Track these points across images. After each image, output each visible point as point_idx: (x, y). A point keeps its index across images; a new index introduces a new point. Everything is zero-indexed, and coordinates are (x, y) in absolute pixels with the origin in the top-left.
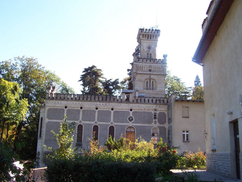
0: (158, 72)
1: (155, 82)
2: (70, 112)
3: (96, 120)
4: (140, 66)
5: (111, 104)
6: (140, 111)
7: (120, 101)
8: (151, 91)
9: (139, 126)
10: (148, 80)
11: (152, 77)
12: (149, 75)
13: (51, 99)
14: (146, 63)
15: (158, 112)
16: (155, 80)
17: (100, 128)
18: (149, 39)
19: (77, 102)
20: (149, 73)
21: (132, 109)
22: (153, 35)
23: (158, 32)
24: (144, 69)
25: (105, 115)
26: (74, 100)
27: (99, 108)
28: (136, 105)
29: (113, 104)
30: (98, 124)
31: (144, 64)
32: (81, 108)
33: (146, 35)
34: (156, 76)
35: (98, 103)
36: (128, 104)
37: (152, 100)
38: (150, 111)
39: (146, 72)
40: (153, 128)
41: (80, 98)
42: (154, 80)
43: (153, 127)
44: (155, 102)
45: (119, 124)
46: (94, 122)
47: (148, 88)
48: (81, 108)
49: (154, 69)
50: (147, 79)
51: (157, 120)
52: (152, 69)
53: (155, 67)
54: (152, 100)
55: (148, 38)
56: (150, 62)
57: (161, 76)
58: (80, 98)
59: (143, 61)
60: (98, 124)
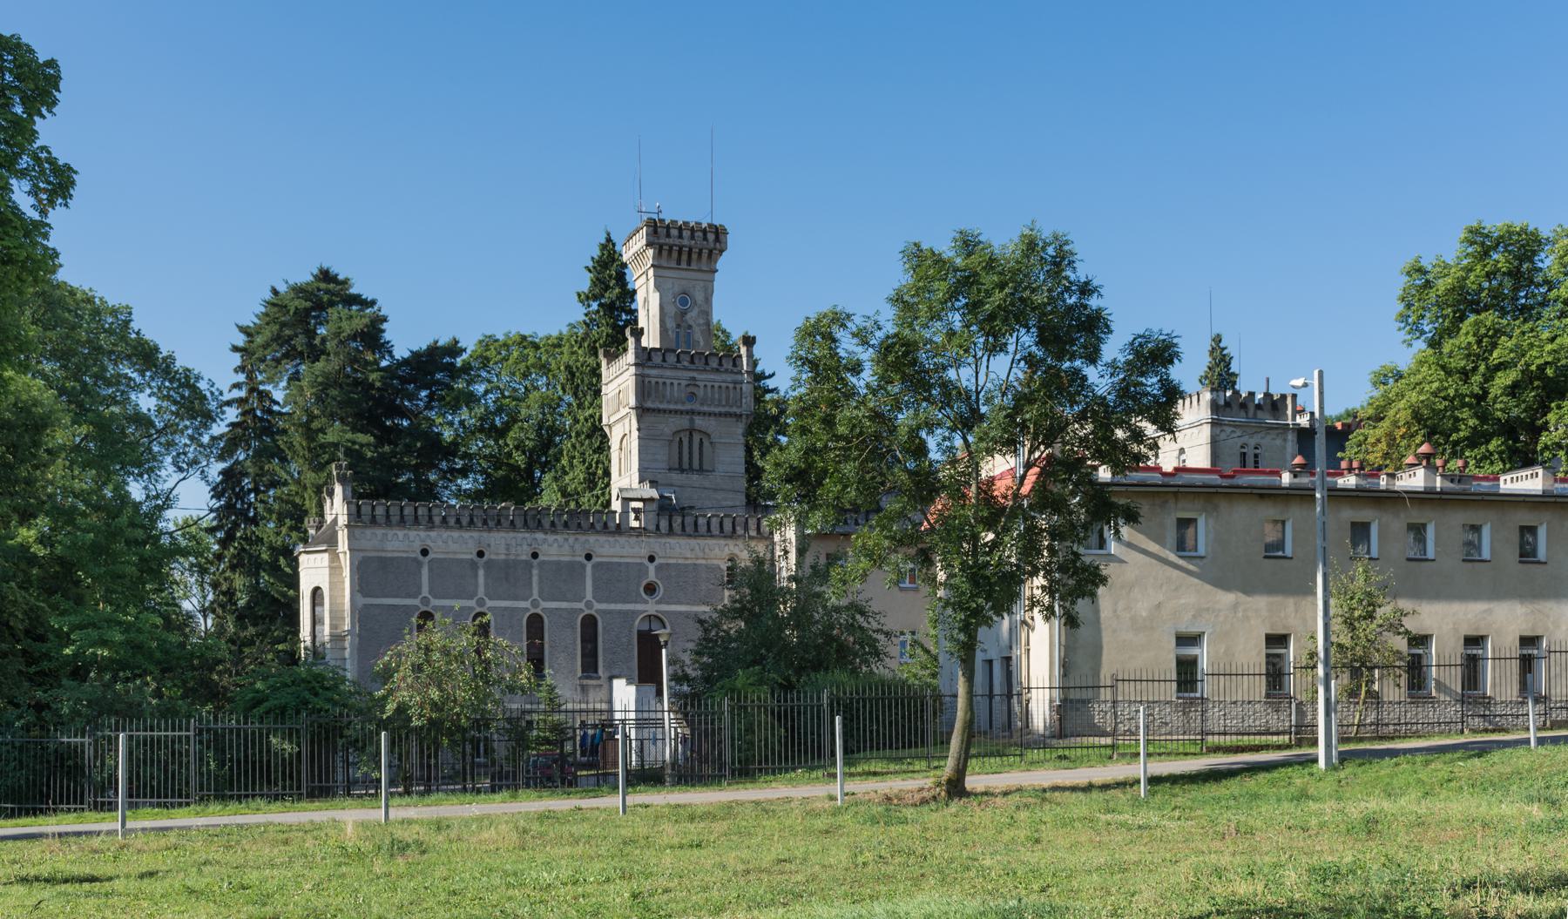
1: (711, 443)
2: (440, 569)
3: (589, 596)
4: (653, 381)
5: (582, 538)
6: (680, 561)
8: (695, 477)
9: (680, 613)
10: (682, 435)
11: (699, 422)
12: (688, 417)
14: (676, 368)
16: (709, 435)
17: (550, 622)
18: (684, 265)
19: (466, 535)
20: (688, 407)
22: (701, 250)
23: (722, 237)
24: (668, 393)
25: (565, 577)
26: (452, 527)
28: (668, 540)
29: (592, 538)
31: (668, 373)
32: (535, 555)
33: (671, 247)
34: (712, 418)
35: (540, 536)
37: (721, 524)
38: (715, 562)
39: (676, 403)
42: (705, 433)
44: (731, 529)
45: (612, 607)
46: (427, 595)
47: (686, 466)
48: (535, 555)
49: (705, 393)
50: (679, 431)
52: (700, 393)
53: (709, 384)
54: (721, 524)
55: (679, 262)
56: (693, 367)
57: (729, 419)
58: (475, 520)
59: (664, 360)
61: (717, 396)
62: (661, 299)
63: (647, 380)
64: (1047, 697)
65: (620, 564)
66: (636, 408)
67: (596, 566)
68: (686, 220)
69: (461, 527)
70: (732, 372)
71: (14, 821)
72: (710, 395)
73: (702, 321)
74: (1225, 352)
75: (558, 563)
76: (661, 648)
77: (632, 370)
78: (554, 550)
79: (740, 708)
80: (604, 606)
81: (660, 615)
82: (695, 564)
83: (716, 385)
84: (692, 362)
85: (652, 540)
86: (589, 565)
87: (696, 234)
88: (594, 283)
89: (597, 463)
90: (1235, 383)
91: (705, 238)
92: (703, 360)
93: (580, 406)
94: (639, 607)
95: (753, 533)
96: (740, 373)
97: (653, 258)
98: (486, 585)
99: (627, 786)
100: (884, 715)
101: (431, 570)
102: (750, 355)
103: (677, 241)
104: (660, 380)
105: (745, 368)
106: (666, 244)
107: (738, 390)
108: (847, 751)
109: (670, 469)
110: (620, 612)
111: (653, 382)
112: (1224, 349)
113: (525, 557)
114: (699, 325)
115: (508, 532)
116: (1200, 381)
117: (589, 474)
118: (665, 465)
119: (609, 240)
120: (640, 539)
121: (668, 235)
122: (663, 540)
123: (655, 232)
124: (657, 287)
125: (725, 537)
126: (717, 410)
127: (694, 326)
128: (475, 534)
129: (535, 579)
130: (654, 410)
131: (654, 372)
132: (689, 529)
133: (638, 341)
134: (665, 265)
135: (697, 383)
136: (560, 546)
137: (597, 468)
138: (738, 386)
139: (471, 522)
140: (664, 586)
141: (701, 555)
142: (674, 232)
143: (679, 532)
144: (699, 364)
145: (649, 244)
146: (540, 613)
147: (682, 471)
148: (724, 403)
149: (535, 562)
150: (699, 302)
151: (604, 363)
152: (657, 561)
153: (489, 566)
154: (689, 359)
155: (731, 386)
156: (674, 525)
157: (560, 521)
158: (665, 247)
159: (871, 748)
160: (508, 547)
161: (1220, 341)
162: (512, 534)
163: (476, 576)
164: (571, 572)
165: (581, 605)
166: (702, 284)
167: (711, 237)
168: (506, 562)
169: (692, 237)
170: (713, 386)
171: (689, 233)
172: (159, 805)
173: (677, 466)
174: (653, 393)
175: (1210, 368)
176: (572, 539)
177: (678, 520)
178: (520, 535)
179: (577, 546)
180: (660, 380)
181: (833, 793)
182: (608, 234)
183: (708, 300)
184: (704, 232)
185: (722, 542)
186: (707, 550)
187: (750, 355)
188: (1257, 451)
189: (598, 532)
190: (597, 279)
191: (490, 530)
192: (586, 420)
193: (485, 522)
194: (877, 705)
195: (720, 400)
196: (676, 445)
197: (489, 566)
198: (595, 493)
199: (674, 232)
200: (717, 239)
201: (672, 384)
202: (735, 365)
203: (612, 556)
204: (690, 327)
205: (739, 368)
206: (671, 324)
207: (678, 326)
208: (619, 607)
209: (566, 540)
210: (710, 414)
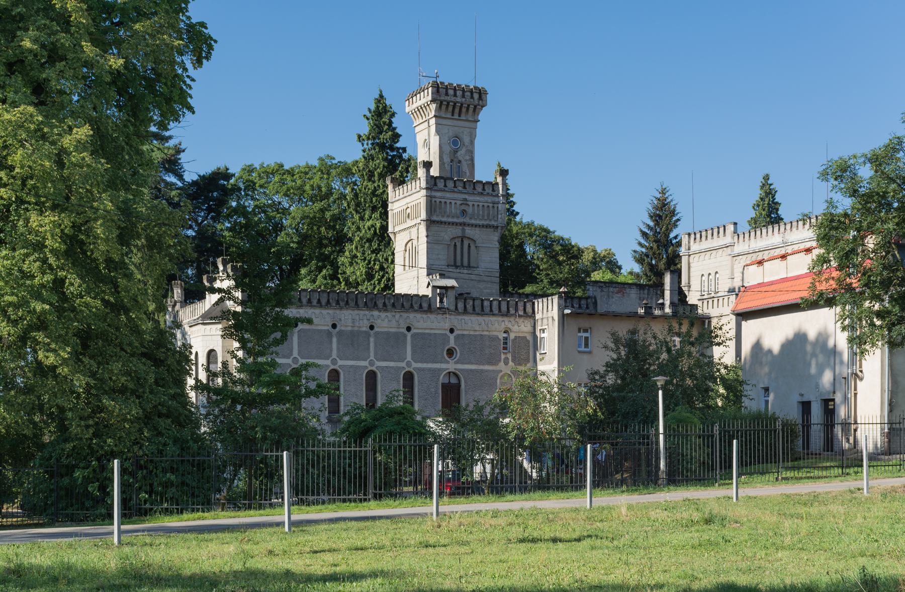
0: (483, 219)
3: (409, 358)
4: (438, 200)
5: (405, 315)
6: (472, 333)
7: (426, 309)
9: (471, 370)
10: (456, 241)
11: (469, 232)
14: (454, 192)
15: (512, 336)
16: (474, 241)
17: (382, 376)
18: (456, 116)
19: (325, 312)
20: (461, 220)
22: (469, 106)
23: (483, 96)
26: (315, 306)
28: (464, 317)
29: (412, 315)
31: (448, 195)
32: (372, 327)
33: (448, 103)
35: (376, 313)
38: (495, 333)
39: (453, 217)
41: (328, 301)
43: (501, 371)
44: (506, 310)
45: (425, 365)
47: (459, 263)
48: (372, 327)
49: (473, 210)
50: (454, 238)
51: (509, 356)
52: (470, 210)
53: (476, 204)
55: (453, 115)
56: (465, 191)
59: (445, 186)
61: (481, 213)
62: (440, 141)
63: (434, 200)
64: (879, 430)
65: (430, 334)
66: (427, 220)
67: (414, 336)
68: (459, 83)
69: (321, 306)
70: (492, 195)
71: (262, 512)
72: (476, 212)
73: (468, 158)
74: (771, 187)
75: (388, 333)
76: (658, 389)
77: (424, 192)
78: (385, 323)
79: (725, 432)
80: (420, 365)
81: (457, 372)
83: (481, 204)
84: (464, 187)
85: (452, 317)
86: (409, 335)
87: (466, 94)
88: (372, 128)
89: (375, 260)
90: (777, 210)
91: (472, 97)
93: (362, 218)
94: (443, 366)
95: (521, 313)
96: (497, 196)
97: (436, 111)
98: (338, 349)
99: (594, 487)
100: (767, 440)
101: (299, 338)
102: (505, 184)
103: (453, 99)
104: (443, 201)
105: (501, 192)
106: (445, 101)
107: (496, 209)
108: (741, 464)
109: (448, 266)
110: (430, 369)
111: (438, 202)
112: (771, 185)
113: (365, 329)
114: (466, 160)
115: (354, 310)
116: (753, 207)
117: (368, 268)
118: (445, 263)
119: (381, 96)
120: (445, 316)
121: (447, 94)
122: (460, 317)
123: (438, 91)
124: (438, 132)
125: (502, 315)
126: (481, 223)
127: (463, 161)
128: (331, 312)
130: (438, 222)
131: (438, 194)
132: (478, 309)
133: (428, 171)
134: (444, 116)
135: (468, 203)
136: (389, 321)
137: (375, 264)
138: (496, 206)
139: (328, 302)
141: (486, 328)
142: (451, 92)
144: (469, 188)
145: (433, 101)
147: (457, 267)
148: (486, 218)
149: (372, 332)
150: (466, 144)
151: (390, 187)
152: (456, 332)
153: (340, 334)
155: (491, 205)
156: (468, 306)
159: (759, 463)
160: (353, 321)
161: (768, 179)
162: (356, 312)
163: (331, 342)
164: (398, 339)
165: (403, 364)
166: (468, 130)
167: (476, 96)
168: (352, 332)
169: (463, 96)
170: (478, 205)
171: (461, 92)
172: (344, 501)
174: (438, 211)
175: (762, 199)
176: (398, 315)
177: (470, 303)
178: (362, 312)
179: (401, 321)
180: (443, 201)
181: (730, 495)
182: (381, 92)
183: (472, 142)
184: (471, 92)
185: (500, 319)
186: (490, 325)
187: (505, 184)
189: (416, 311)
190: (375, 125)
191: (341, 308)
192: (369, 229)
193: (338, 303)
194: (758, 434)
195: (483, 216)
196: (452, 248)
198: (372, 282)
199: (451, 92)
200: (480, 98)
201: (450, 203)
202: (493, 190)
203: (425, 329)
204: (460, 162)
205: (496, 193)
206: (447, 160)
207: (452, 161)
208: (430, 366)
210: (476, 226)
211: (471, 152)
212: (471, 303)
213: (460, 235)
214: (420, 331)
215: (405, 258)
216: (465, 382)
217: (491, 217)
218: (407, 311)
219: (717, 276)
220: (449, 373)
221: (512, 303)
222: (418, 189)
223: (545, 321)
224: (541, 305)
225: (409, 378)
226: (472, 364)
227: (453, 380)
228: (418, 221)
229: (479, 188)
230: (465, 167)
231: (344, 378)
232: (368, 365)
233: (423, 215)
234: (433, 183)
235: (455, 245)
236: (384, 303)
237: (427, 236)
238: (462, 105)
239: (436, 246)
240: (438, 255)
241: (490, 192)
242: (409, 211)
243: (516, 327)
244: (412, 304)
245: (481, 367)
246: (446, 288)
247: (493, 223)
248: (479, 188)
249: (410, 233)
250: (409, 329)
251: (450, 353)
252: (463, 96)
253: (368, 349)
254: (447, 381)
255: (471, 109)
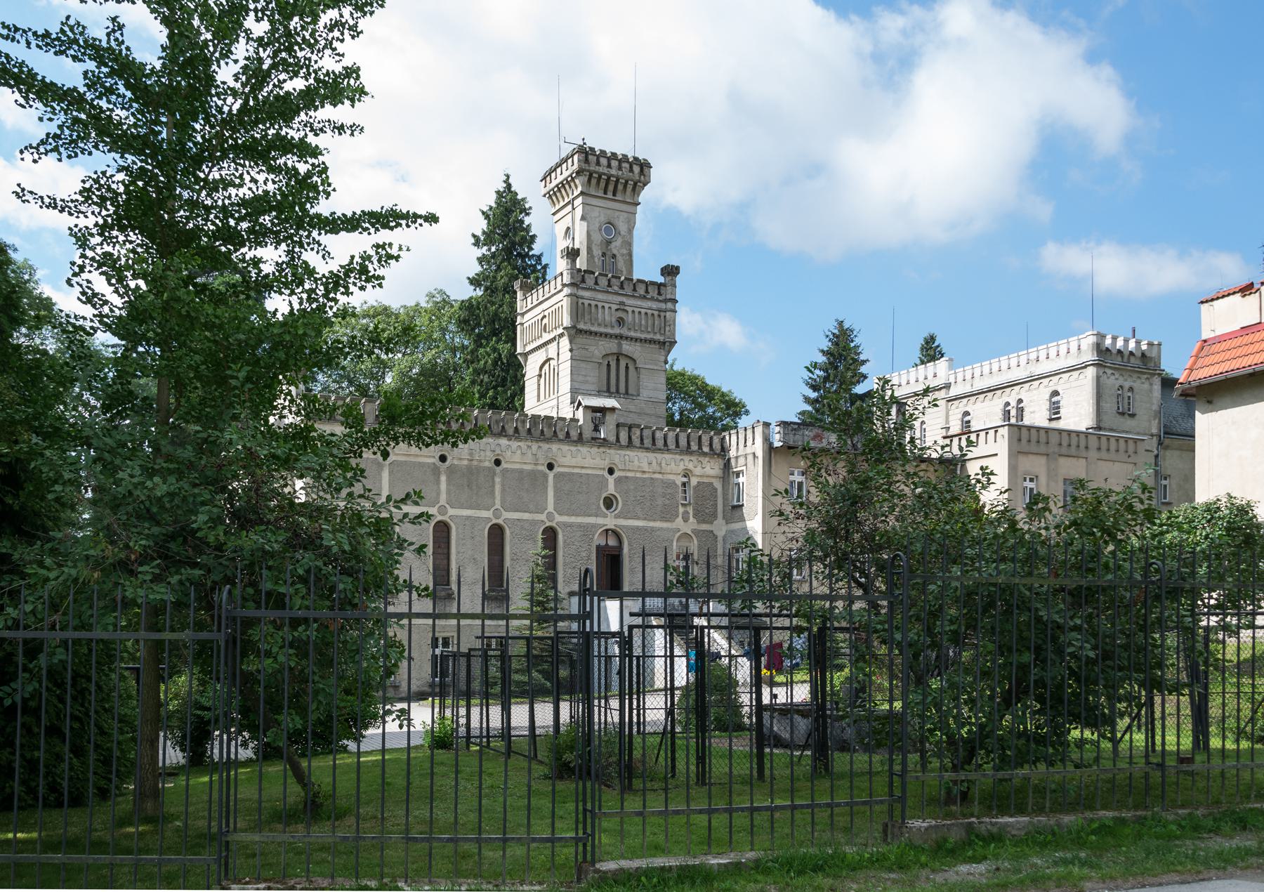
3: (550, 508)
4: (586, 302)
5: (545, 446)
6: (639, 475)
7: (575, 439)
9: (638, 528)
10: (610, 358)
11: (627, 347)
13: (575, 441)
15: (694, 481)
16: (634, 361)
18: (610, 195)
20: (617, 331)
21: (500, 458)
22: (627, 182)
23: (646, 170)
27: (559, 466)
28: (628, 453)
29: (555, 447)
30: (503, 518)
31: (600, 296)
32: (498, 463)
33: (600, 177)
36: (602, 449)
38: (671, 477)
40: (679, 534)
42: (631, 358)
44: (686, 444)
45: (573, 519)
47: (613, 389)
48: (498, 463)
50: (607, 355)
53: (637, 310)
55: (605, 193)
60: (503, 518)
61: (643, 322)
65: (581, 475)
70: (658, 300)
73: (625, 252)
75: (521, 471)
80: (565, 519)
82: (652, 479)
84: (622, 287)
85: (612, 451)
86: (551, 475)
92: (632, 287)
94: (600, 521)
95: (706, 449)
98: (448, 492)
101: (391, 473)
103: (606, 170)
106: (596, 172)
110: (580, 525)
114: (623, 255)
122: (622, 452)
126: (643, 336)
129: (498, 488)
130: (586, 332)
131: (586, 294)
132: (647, 442)
135: (626, 308)
136: (523, 454)
140: (623, 501)
143: (638, 445)
144: (628, 289)
146: (502, 523)
149: (498, 469)
150: (622, 233)
152: (617, 474)
153: (452, 471)
154: (619, 284)
156: (633, 437)
157: (523, 427)
158: (595, 175)
163: (438, 482)
165: (543, 517)
167: (636, 169)
168: (469, 468)
170: (640, 312)
171: (617, 163)
173: (605, 389)
176: (535, 446)
179: (540, 454)
180: (593, 303)
183: (630, 231)
186: (663, 465)
188: (967, 418)
196: (605, 368)
197: (452, 471)
201: (603, 307)
204: (614, 256)
206: (597, 252)
207: (604, 255)
208: (580, 520)
209: (529, 447)
210: (636, 340)
211: (628, 244)
212: (638, 433)
213: (615, 351)
214: (566, 470)
215: (539, 385)
216: (629, 544)
217: (656, 330)
218: (548, 440)
219: (924, 426)
220: (607, 531)
221: (694, 436)
222: (559, 287)
223: (741, 461)
224: (734, 438)
225: (550, 536)
226: (638, 518)
227: (612, 542)
228: (560, 331)
229: (641, 290)
230: (621, 264)
231: (457, 535)
232: (491, 516)
233: (567, 321)
234: (580, 279)
235: (609, 365)
236: (516, 428)
237: (571, 350)
238: (617, 181)
239: (583, 365)
240: (585, 376)
241: (656, 296)
242: (545, 321)
243: (699, 468)
244: (555, 432)
245: (651, 524)
246: (602, 410)
247: (658, 337)
248: (641, 290)
249: (547, 351)
250: (550, 466)
251: (609, 503)
252: (620, 168)
253: (493, 492)
254: (603, 543)
255: (630, 188)
